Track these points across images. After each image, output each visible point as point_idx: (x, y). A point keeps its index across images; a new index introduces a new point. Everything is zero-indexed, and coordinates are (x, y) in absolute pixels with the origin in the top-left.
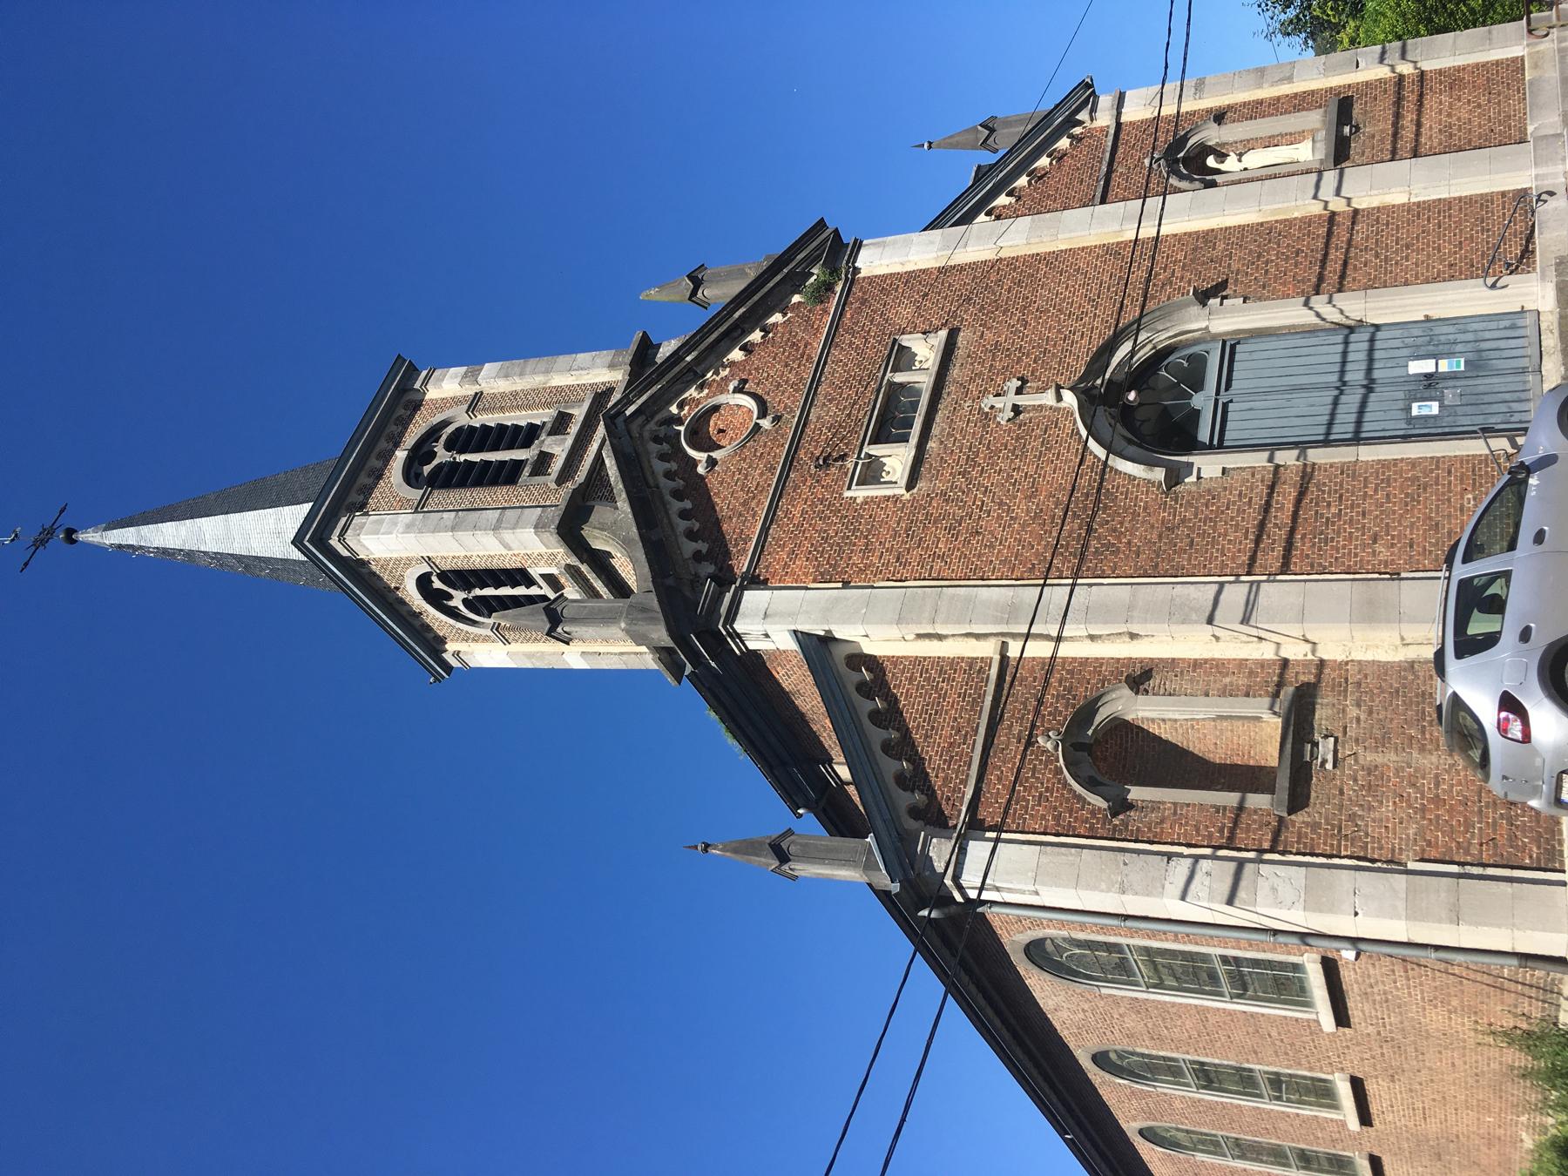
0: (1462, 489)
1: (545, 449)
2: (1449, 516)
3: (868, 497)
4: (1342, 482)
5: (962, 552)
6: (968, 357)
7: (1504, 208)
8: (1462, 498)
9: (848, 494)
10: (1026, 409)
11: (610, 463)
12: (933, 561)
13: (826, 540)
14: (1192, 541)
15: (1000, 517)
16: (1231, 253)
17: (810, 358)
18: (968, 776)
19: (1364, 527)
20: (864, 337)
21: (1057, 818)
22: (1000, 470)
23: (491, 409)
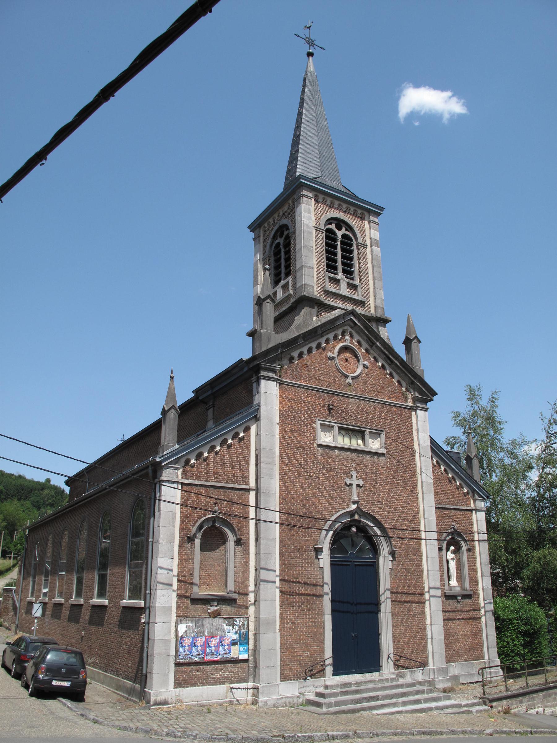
1: (341, 281)
2: (301, 647)
4: (316, 610)
6: (374, 463)
7: (421, 658)
8: (308, 651)
10: (351, 489)
11: (336, 313)
15: (305, 484)
17: (377, 395)
19: (298, 619)
20: (385, 417)
22: (325, 482)
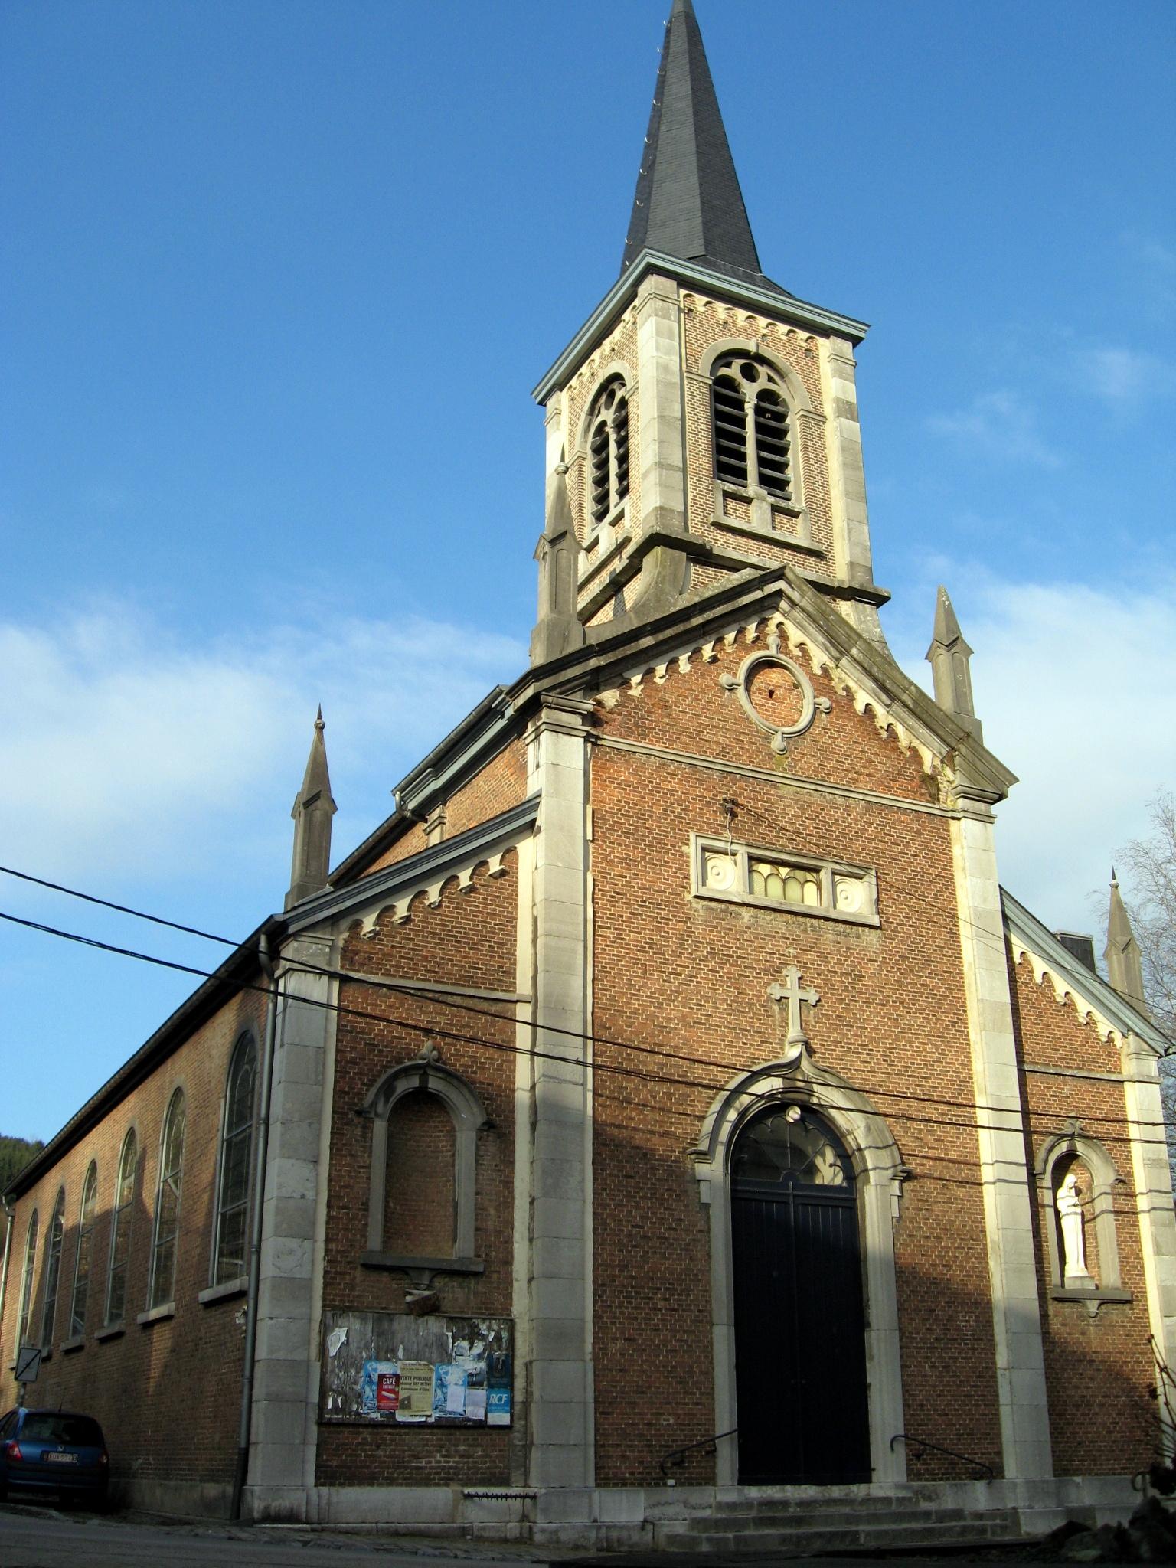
0: (680, 1415)
3: (688, 857)
4: (690, 1311)
5: (624, 957)
6: (848, 948)
8: (670, 1414)
9: (692, 836)
12: (615, 929)
13: (642, 818)
14: (631, 1177)
15: (662, 992)
16: (952, 1203)
18: (394, 976)
19: (643, 1330)
21: (353, 1062)
23: (805, 437)
